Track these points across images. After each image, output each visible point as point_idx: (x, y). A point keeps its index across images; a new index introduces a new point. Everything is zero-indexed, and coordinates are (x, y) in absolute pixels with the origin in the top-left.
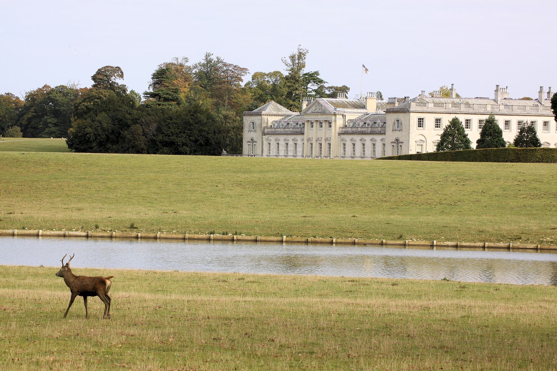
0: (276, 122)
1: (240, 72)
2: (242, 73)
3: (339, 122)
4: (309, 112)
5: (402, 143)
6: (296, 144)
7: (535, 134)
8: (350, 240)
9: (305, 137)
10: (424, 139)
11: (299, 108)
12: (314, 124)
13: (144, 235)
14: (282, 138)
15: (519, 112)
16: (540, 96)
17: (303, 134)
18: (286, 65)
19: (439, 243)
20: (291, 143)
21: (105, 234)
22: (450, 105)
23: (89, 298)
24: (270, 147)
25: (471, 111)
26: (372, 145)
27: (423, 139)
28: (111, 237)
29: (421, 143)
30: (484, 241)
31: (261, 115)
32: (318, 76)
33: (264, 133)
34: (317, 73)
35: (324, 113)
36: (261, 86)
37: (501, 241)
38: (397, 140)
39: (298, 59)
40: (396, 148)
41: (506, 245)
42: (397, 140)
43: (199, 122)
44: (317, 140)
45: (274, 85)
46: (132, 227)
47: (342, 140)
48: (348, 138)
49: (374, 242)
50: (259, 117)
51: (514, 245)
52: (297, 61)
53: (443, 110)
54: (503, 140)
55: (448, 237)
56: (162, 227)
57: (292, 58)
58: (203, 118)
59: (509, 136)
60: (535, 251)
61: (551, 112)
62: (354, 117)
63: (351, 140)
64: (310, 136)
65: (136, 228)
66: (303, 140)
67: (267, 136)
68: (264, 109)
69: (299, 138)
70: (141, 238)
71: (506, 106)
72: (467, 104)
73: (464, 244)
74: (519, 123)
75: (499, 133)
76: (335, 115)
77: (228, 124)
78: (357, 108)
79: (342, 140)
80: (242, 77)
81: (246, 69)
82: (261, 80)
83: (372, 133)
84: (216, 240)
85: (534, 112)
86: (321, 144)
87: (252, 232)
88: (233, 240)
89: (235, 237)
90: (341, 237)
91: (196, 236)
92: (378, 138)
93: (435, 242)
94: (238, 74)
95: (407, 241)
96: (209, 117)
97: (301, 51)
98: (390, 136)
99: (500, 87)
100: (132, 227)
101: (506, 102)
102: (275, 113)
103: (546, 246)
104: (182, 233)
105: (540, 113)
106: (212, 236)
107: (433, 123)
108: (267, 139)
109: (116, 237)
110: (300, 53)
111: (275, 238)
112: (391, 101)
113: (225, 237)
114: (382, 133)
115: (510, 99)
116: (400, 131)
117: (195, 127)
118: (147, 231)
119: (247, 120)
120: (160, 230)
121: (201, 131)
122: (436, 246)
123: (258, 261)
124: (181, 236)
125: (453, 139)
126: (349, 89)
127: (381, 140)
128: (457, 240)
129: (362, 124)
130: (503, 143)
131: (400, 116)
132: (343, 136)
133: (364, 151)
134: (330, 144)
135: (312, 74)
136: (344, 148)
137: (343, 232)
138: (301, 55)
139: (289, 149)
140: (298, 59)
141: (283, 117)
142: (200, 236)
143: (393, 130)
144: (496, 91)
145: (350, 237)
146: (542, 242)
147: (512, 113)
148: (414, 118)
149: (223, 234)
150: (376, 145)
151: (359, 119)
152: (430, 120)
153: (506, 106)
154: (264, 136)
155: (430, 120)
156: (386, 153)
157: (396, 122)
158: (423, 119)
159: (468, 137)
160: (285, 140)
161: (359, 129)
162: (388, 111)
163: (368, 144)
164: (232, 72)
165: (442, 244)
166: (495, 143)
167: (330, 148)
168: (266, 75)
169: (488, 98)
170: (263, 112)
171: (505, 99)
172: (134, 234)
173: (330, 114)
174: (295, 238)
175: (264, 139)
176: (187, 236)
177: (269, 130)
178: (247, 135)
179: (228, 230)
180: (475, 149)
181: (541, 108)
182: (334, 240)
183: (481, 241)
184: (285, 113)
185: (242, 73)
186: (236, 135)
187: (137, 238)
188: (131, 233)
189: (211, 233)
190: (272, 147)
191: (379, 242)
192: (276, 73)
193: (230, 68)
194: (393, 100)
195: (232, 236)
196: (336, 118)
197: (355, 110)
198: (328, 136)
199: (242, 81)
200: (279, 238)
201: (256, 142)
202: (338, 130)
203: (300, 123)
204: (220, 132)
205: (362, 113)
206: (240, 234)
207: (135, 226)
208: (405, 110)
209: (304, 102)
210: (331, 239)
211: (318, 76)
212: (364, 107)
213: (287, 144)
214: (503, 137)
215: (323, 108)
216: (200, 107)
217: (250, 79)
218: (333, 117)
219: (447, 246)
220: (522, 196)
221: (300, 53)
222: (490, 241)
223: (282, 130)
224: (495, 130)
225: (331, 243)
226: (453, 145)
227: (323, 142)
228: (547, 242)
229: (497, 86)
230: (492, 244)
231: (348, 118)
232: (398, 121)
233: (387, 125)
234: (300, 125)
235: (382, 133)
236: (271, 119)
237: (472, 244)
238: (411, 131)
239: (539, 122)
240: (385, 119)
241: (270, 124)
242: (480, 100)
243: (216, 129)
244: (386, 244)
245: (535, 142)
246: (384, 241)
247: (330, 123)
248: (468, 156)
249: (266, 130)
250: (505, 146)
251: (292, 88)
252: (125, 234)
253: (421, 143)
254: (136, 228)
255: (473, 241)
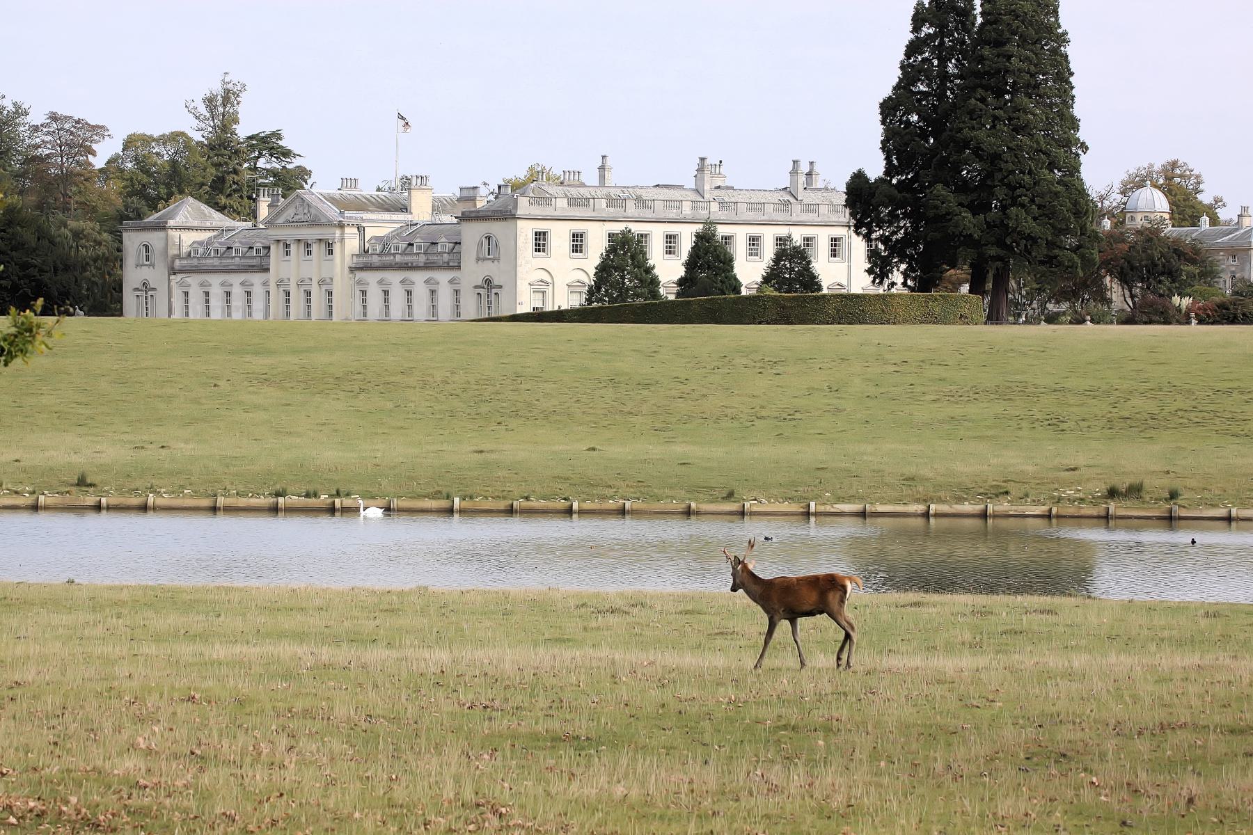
0: (201, 243)
1: (88, 134)
2: (95, 137)
3: (352, 243)
4: (280, 221)
5: (501, 287)
6: (249, 293)
7: (809, 263)
8: (611, 504)
9: (272, 276)
10: (548, 279)
11: (253, 215)
12: (293, 248)
13: (114, 501)
14: (215, 280)
15: (750, 216)
16: (794, 182)
17: (267, 270)
18: (197, 118)
19: (822, 508)
20: (238, 292)
21: (19, 501)
22: (604, 203)
23: (801, 621)
24: (187, 301)
25: (648, 214)
26: (429, 293)
27: (547, 278)
28: (35, 508)
29: (541, 288)
30: (926, 500)
31: (165, 228)
32: (280, 142)
33: (173, 268)
34: (277, 135)
35: (314, 222)
36: (143, 165)
37: (966, 499)
38: (488, 282)
39: (223, 104)
40: (484, 297)
41: (978, 508)
42: (488, 282)
43: (20, 246)
44: (301, 283)
45: (173, 163)
46: (82, 482)
47: (359, 282)
48: (372, 278)
49: (670, 507)
50: (161, 234)
51: (996, 508)
52: (221, 109)
53: (587, 213)
54: (736, 279)
55: (840, 493)
56: (155, 482)
57: (210, 102)
58: (29, 236)
59: (749, 272)
60: (1103, 521)
61: (845, 216)
62: (383, 231)
63: (380, 282)
64: (283, 275)
65: (91, 485)
66: (265, 284)
67: (179, 277)
68: (171, 215)
69: (256, 279)
70: (108, 508)
71: (722, 203)
72: (640, 201)
73: (881, 508)
74: (780, 240)
75: (727, 262)
76: (341, 226)
77: (84, 251)
78: (388, 210)
79: (359, 282)
80: (94, 146)
81: (102, 127)
82: (142, 151)
83: (428, 267)
84: (291, 510)
85: (781, 217)
86: (309, 293)
87: (374, 490)
88: (332, 510)
89: (338, 502)
90: (591, 497)
91: (242, 502)
92: (443, 277)
93: (813, 504)
94: (85, 140)
95: (747, 505)
96: (42, 235)
97: (230, 86)
98: (472, 272)
99: (708, 162)
100: (82, 482)
101: (722, 194)
102: (196, 223)
103: (1071, 511)
104: (208, 496)
105: (795, 218)
106: (281, 500)
107: (567, 244)
108: (181, 284)
109: (46, 508)
110: (227, 92)
111: (434, 504)
112: (465, 194)
113: (312, 502)
114: (454, 265)
115: (728, 188)
116: (493, 260)
117: (12, 258)
118: (120, 490)
119: (132, 241)
120: (152, 489)
121: (25, 266)
122: (816, 514)
123: (470, 555)
124: (206, 502)
125: (623, 277)
126: (309, 173)
127: (451, 282)
128: (862, 499)
129: (405, 245)
130: (735, 286)
131: (495, 228)
132: (359, 275)
133: (410, 307)
134: (330, 293)
135: (267, 136)
136: (364, 301)
137: (590, 485)
138: (229, 96)
139: (233, 304)
140: (223, 104)
141: (215, 233)
142: (254, 502)
143: (478, 259)
144: (701, 170)
145: (612, 498)
146: (1059, 499)
147: (736, 219)
148: (526, 230)
149: (307, 496)
150: (233, 297)
151: (397, 234)
152: (560, 235)
153: (722, 203)
154: (172, 277)
155: (560, 235)
156: (462, 310)
157: (485, 242)
158: (544, 233)
159: (656, 271)
160: (222, 284)
161: (398, 258)
162: (465, 218)
163: (421, 292)
164: (72, 133)
165: (828, 508)
166: (719, 285)
167: (330, 301)
168: (154, 140)
169: (681, 187)
170: (171, 223)
171: (718, 187)
172: (91, 500)
173: (330, 224)
174: (480, 502)
175: (173, 283)
176: (221, 501)
177: (184, 262)
178: (132, 276)
179: (319, 487)
180: (672, 297)
181: (797, 208)
182: (575, 506)
183: (918, 501)
184: (219, 224)
185: (95, 137)
186: (103, 275)
187: (98, 508)
188: (82, 494)
189: (278, 495)
190: (213, 302)
191: (681, 507)
192: (175, 137)
193: (67, 126)
194: (471, 193)
195: (329, 501)
196: (343, 233)
197: (386, 216)
198: (325, 275)
199: (94, 153)
200: (443, 504)
201: (154, 289)
202: (348, 262)
203: (259, 245)
204: (67, 268)
205: (400, 222)
206: (348, 495)
207: (89, 481)
208: (504, 214)
209: (261, 198)
210: (568, 503)
211: (280, 142)
212: (405, 209)
213: (228, 294)
214: (736, 271)
215: (313, 211)
216: (19, 211)
217: (118, 149)
218: (338, 232)
219: (841, 514)
220: (928, 397)
221: (227, 92)
222: (940, 501)
223: (216, 262)
224: (718, 256)
225: (569, 512)
226: (620, 289)
227: (293, 289)
228: (1071, 500)
229: (703, 159)
230: (944, 508)
231: (370, 232)
232: (489, 238)
233: (464, 247)
234: (258, 251)
235: (454, 265)
236: (189, 238)
237: (899, 508)
238: (519, 262)
239: (823, 238)
240: (459, 233)
241: (185, 250)
242: (666, 190)
243: (58, 262)
244: (698, 513)
245: (810, 282)
246: (693, 505)
247: (330, 245)
248: (654, 311)
249: (177, 263)
250: (739, 292)
251: (229, 167)
252: (68, 500)
253: (543, 288)
254: (91, 485)
255: (898, 500)
